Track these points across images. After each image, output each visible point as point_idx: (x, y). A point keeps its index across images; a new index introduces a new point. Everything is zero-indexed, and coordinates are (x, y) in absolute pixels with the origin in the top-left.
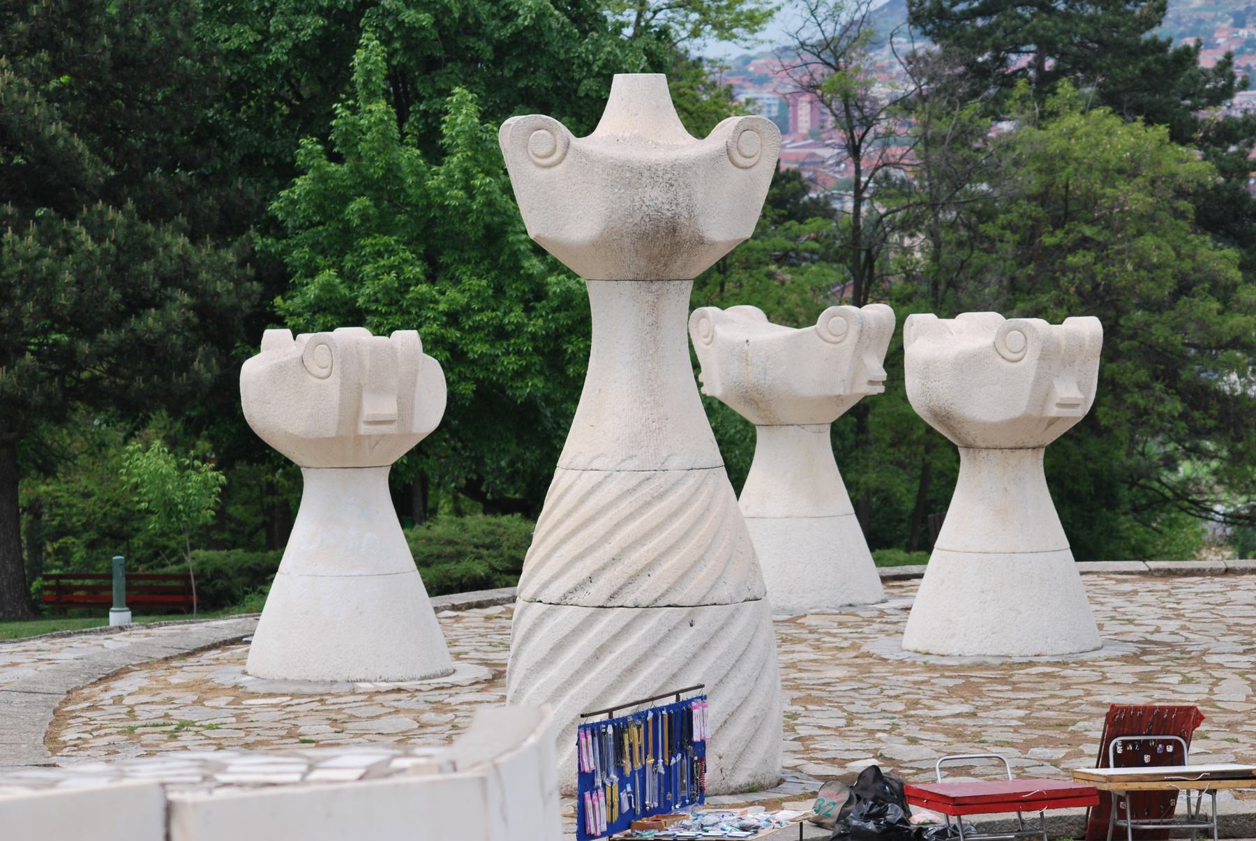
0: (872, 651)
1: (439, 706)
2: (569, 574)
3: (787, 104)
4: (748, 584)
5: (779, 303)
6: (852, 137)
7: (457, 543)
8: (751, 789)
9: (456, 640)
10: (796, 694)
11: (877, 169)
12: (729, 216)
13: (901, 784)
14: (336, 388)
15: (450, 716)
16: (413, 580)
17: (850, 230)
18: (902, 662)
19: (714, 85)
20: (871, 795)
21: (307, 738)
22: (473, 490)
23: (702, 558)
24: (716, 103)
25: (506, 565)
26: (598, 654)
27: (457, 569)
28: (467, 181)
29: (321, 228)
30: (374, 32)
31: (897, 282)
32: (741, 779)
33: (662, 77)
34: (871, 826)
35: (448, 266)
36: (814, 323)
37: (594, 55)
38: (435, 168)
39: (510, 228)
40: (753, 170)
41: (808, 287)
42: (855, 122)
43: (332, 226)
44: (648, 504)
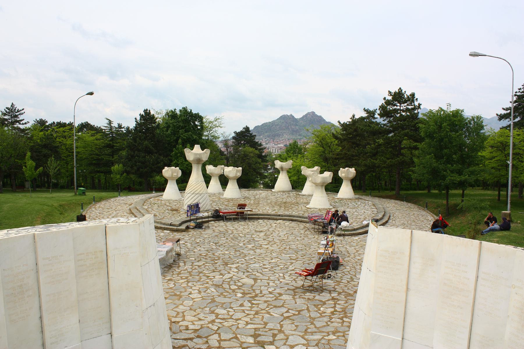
14: (171, 172)
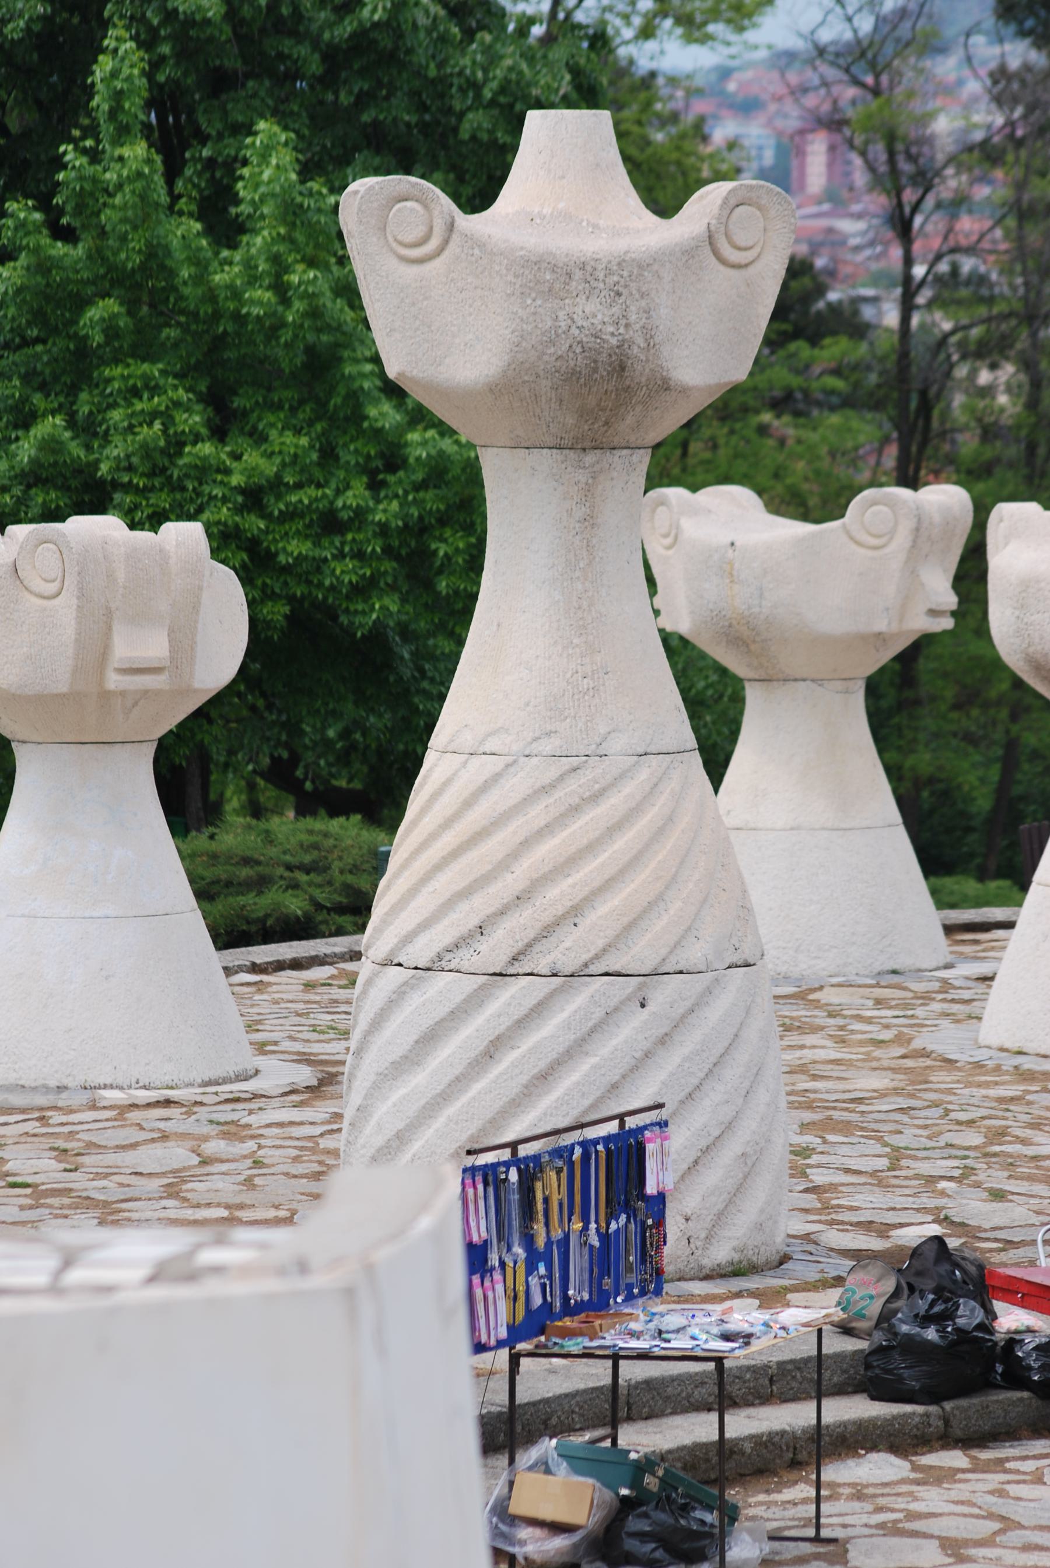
0: (930, 1047)
1: (233, 1129)
2: (446, 922)
3: (791, 149)
4: (735, 941)
5: (776, 476)
6: (900, 205)
7: (258, 863)
8: (737, 1271)
9: (259, 1022)
10: (808, 1116)
11: (938, 257)
12: (711, 346)
13: (981, 1267)
15: (251, 1145)
16: (192, 924)
17: (894, 357)
18: (978, 1065)
19: (674, 117)
20: (931, 1284)
21: (19, 1179)
22: (282, 774)
23: (660, 897)
24: (678, 148)
25: (338, 898)
26: (492, 1051)
27: (259, 904)
28: (278, 276)
29: (39, 348)
30: (128, 28)
31: (968, 444)
32: (721, 1254)
33: (604, 117)
34: (931, 1334)
35: (245, 413)
36: (843, 516)
37: (485, 71)
38: (225, 253)
39: (346, 354)
40: (751, 270)
41: (824, 450)
42: (904, 180)
43: (58, 345)
44: (575, 810)
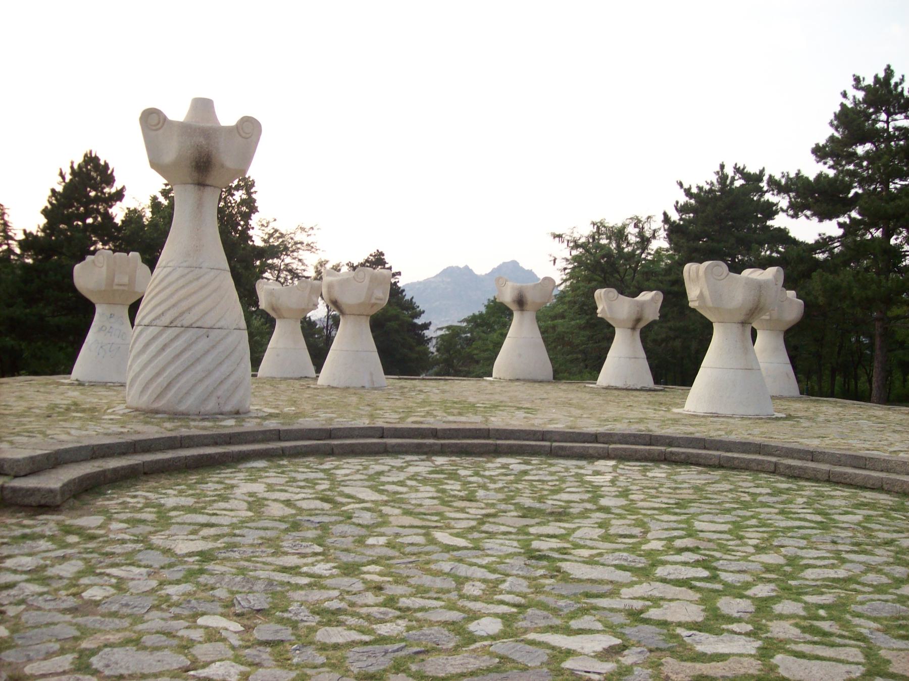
26: (163, 349)
